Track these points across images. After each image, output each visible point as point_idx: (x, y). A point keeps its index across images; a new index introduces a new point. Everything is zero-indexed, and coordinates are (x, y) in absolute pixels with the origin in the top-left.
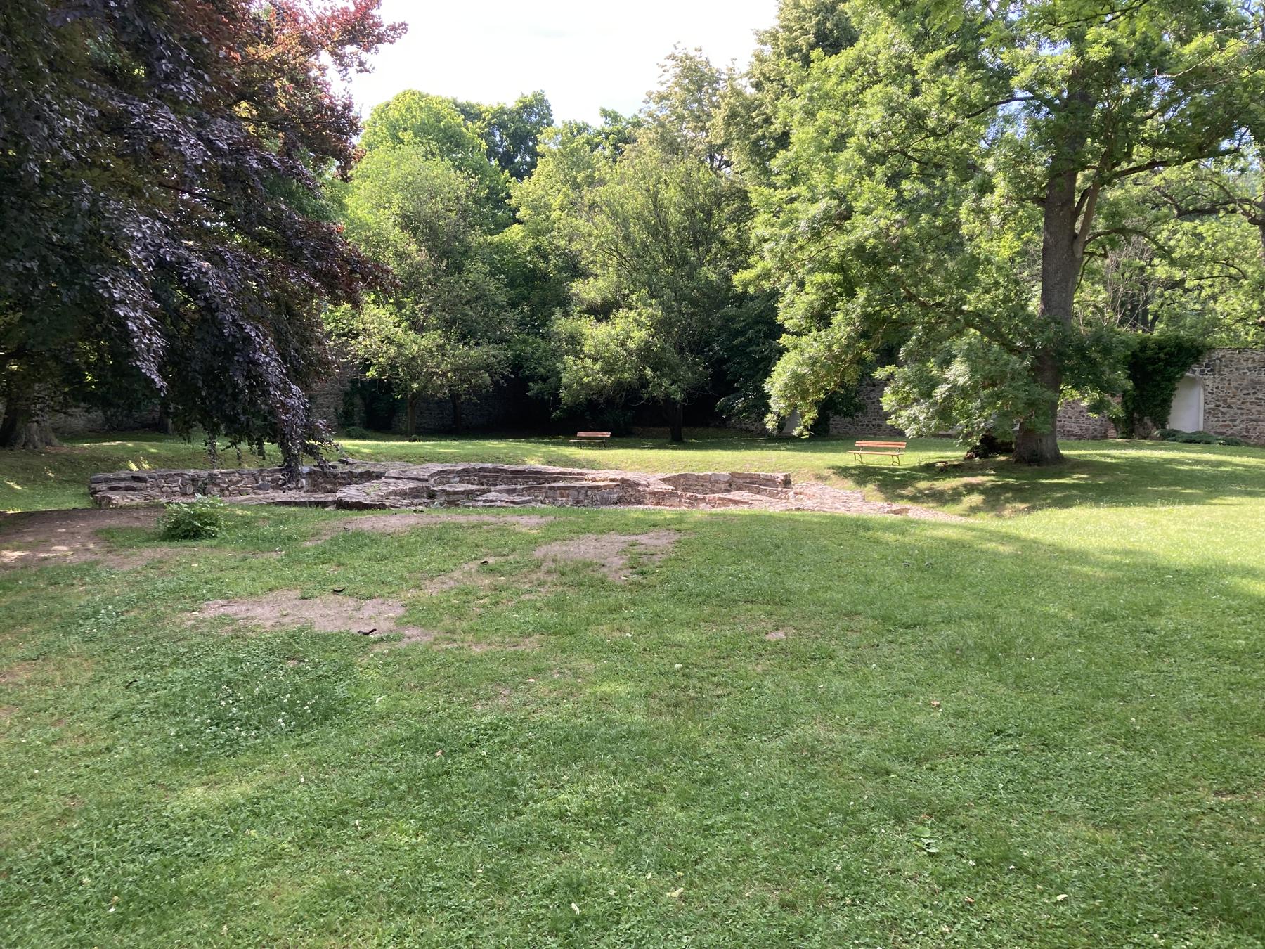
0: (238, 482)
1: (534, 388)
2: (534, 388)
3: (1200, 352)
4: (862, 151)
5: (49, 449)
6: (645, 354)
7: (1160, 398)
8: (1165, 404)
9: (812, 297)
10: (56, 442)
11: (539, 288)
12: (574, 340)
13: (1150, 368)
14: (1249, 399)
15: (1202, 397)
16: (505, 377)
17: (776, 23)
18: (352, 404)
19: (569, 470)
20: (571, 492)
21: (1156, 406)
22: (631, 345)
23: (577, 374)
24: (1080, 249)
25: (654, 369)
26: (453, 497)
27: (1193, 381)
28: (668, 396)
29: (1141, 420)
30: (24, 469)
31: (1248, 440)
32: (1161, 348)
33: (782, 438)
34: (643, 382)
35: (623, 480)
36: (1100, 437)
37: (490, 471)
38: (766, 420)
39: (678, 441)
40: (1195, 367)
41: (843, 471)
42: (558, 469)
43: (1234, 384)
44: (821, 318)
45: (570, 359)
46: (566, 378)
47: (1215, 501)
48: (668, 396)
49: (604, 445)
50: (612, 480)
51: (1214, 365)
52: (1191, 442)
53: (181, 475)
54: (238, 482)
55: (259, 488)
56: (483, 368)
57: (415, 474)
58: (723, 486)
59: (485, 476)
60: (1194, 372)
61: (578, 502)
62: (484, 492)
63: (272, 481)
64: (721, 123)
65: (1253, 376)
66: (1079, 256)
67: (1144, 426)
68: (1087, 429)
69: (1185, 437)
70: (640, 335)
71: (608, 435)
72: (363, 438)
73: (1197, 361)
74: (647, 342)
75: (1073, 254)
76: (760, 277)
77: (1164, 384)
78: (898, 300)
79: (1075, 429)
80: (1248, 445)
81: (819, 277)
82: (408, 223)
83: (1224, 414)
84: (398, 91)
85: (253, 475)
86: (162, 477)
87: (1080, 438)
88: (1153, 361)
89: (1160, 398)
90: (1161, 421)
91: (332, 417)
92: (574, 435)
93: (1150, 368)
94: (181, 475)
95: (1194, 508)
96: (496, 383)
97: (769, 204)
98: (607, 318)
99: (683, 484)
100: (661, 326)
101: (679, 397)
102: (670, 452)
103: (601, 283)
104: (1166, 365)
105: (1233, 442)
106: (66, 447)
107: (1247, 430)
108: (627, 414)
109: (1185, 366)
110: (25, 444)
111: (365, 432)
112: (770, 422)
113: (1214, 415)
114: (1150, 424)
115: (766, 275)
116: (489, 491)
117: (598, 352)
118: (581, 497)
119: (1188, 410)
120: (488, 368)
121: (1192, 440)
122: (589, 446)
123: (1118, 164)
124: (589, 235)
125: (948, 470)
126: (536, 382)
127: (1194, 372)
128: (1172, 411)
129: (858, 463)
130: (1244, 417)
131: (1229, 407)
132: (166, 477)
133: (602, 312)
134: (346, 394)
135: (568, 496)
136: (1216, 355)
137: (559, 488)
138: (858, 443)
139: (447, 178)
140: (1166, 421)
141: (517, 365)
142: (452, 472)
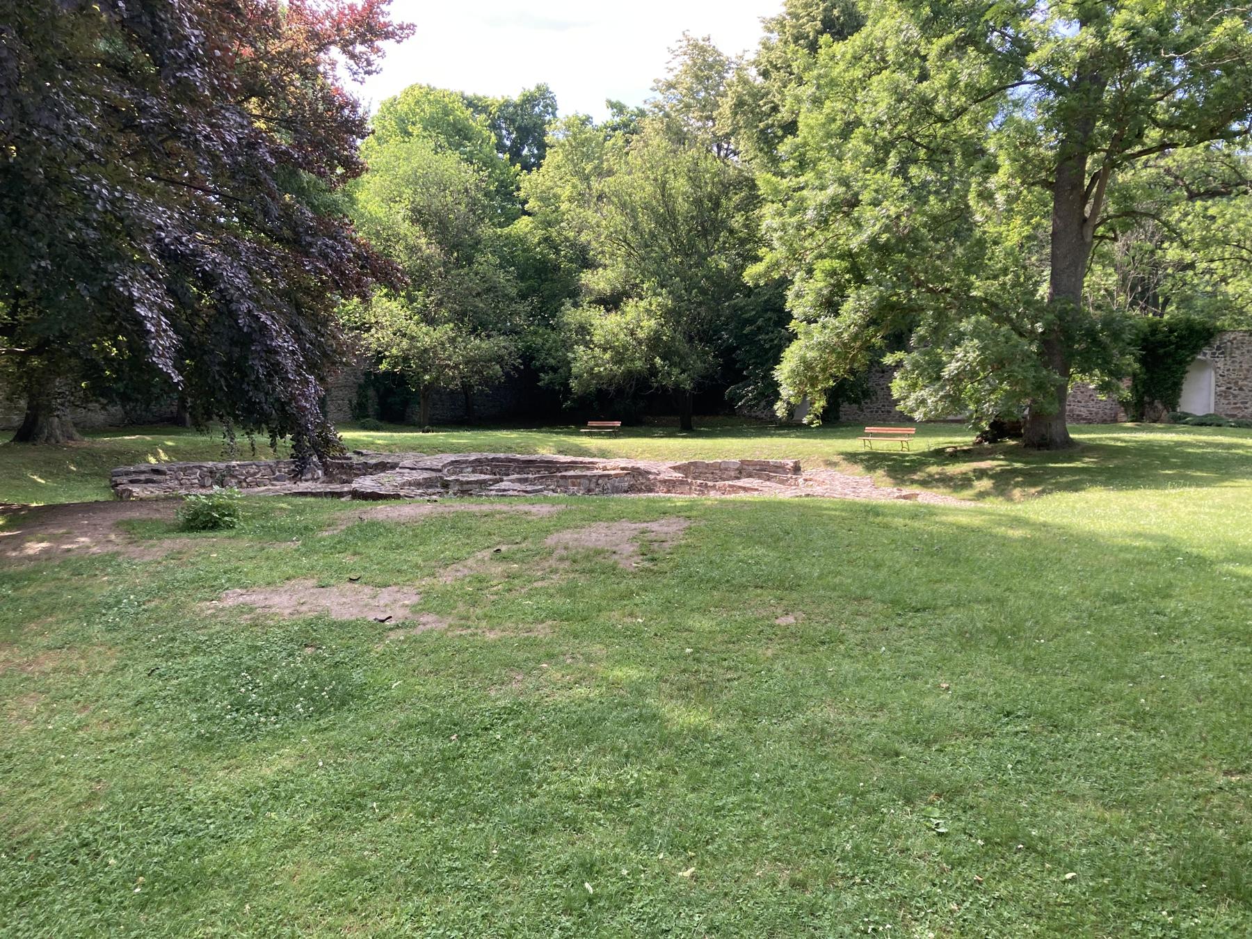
0: (255, 474)
1: (545, 378)
2: (545, 378)
5: (71, 443)
6: (654, 342)
8: (1176, 388)
10: (77, 436)
11: (548, 279)
12: (583, 330)
13: (1161, 351)
15: (1213, 379)
16: (516, 368)
20: (582, 481)
21: (1167, 389)
22: (641, 335)
23: (587, 362)
26: (466, 487)
29: (1151, 403)
30: (47, 463)
35: (633, 469)
36: (1110, 421)
38: (776, 407)
39: (688, 428)
40: (1206, 350)
41: (852, 457)
44: (831, 305)
46: (576, 368)
49: (615, 434)
50: (623, 469)
51: (1225, 348)
52: (1202, 424)
53: (200, 467)
54: (255, 474)
55: (276, 479)
58: (733, 474)
60: (1205, 354)
66: (1088, 240)
67: (1154, 409)
68: (1097, 413)
71: (618, 424)
73: (1208, 343)
75: (1083, 238)
77: (1175, 367)
78: (909, 291)
83: (1235, 396)
85: (270, 467)
87: (1089, 421)
88: (1163, 344)
90: (1172, 403)
91: (346, 409)
93: (1161, 351)
94: (200, 467)
96: (507, 374)
99: (693, 471)
101: (688, 386)
103: (610, 274)
104: (1178, 348)
106: (87, 441)
108: (637, 402)
109: (1196, 349)
112: (780, 409)
113: (1225, 398)
114: (1160, 407)
115: (776, 265)
118: (592, 486)
119: (1199, 393)
120: (500, 360)
121: (1202, 423)
122: (599, 435)
126: (546, 373)
127: (1205, 355)
128: (1183, 393)
129: (867, 449)
131: (1241, 389)
133: (612, 302)
134: (360, 386)
135: (579, 484)
137: (571, 477)
138: (868, 429)
141: (528, 356)
142: (465, 462)
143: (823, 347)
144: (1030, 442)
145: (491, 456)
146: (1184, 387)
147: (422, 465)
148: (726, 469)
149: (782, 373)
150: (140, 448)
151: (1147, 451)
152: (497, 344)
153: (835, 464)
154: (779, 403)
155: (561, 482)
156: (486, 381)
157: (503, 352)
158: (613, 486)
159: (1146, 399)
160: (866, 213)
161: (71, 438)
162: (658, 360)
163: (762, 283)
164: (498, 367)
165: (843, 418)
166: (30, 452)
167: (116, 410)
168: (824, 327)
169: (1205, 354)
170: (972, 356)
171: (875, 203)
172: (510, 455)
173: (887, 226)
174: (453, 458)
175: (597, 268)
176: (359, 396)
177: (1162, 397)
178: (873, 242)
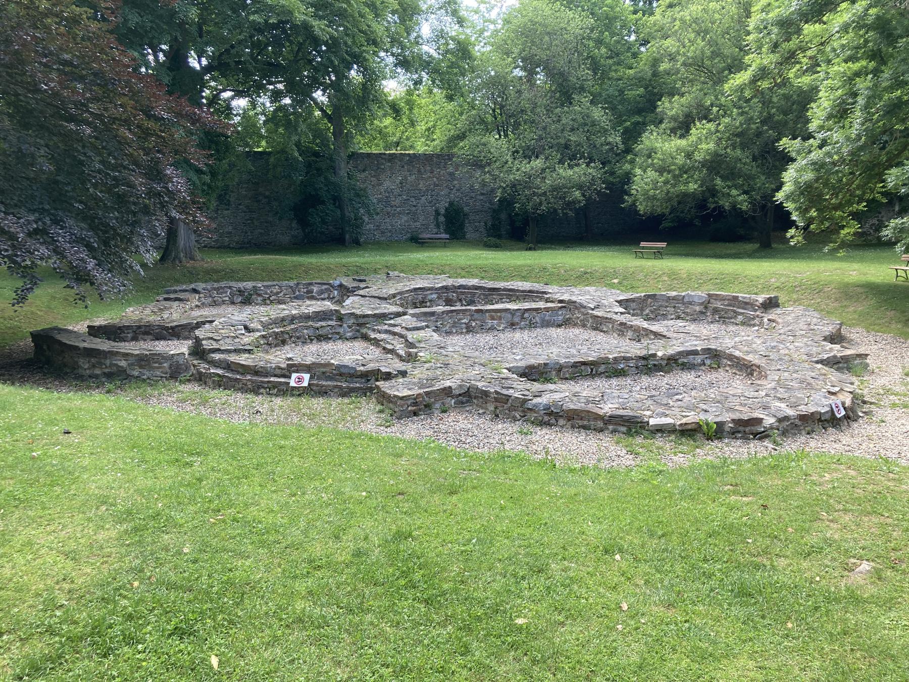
6: (715, 164)
16: (599, 193)
18: (499, 219)
19: (462, 281)
20: (503, 314)
22: (698, 156)
23: (645, 184)
26: (361, 321)
28: (734, 206)
38: (788, 235)
41: (875, 290)
42: (526, 285)
47: (230, 324)
48: (734, 206)
49: (659, 254)
50: (561, 301)
53: (230, 287)
54: (278, 293)
55: (296, 298)
58: (698, 308)
59: (463, 293)
61: (513, 324)
63: (308, 292)
74: (716, 154)
76: (754, 81)
86: (215, 289)
91: (482, 229)
92: (636, 242)
95: (681, 349)
96: (588, 200)
98: (26, 126)
102: (837, 265)
111: (498, 241)
115: (763, 73)
116: (405, 314)
118: (516, 320)
132: (217, 289)
134: (494, 211)
135: (500, 318)
138: (643, 244)
143: (818, 166)
148: (690, 303)
152: (578, 174)
154: (792, 231)
155: (476, 316)
158: (543, 320)
162: (718, 181)
165: (468, 236)
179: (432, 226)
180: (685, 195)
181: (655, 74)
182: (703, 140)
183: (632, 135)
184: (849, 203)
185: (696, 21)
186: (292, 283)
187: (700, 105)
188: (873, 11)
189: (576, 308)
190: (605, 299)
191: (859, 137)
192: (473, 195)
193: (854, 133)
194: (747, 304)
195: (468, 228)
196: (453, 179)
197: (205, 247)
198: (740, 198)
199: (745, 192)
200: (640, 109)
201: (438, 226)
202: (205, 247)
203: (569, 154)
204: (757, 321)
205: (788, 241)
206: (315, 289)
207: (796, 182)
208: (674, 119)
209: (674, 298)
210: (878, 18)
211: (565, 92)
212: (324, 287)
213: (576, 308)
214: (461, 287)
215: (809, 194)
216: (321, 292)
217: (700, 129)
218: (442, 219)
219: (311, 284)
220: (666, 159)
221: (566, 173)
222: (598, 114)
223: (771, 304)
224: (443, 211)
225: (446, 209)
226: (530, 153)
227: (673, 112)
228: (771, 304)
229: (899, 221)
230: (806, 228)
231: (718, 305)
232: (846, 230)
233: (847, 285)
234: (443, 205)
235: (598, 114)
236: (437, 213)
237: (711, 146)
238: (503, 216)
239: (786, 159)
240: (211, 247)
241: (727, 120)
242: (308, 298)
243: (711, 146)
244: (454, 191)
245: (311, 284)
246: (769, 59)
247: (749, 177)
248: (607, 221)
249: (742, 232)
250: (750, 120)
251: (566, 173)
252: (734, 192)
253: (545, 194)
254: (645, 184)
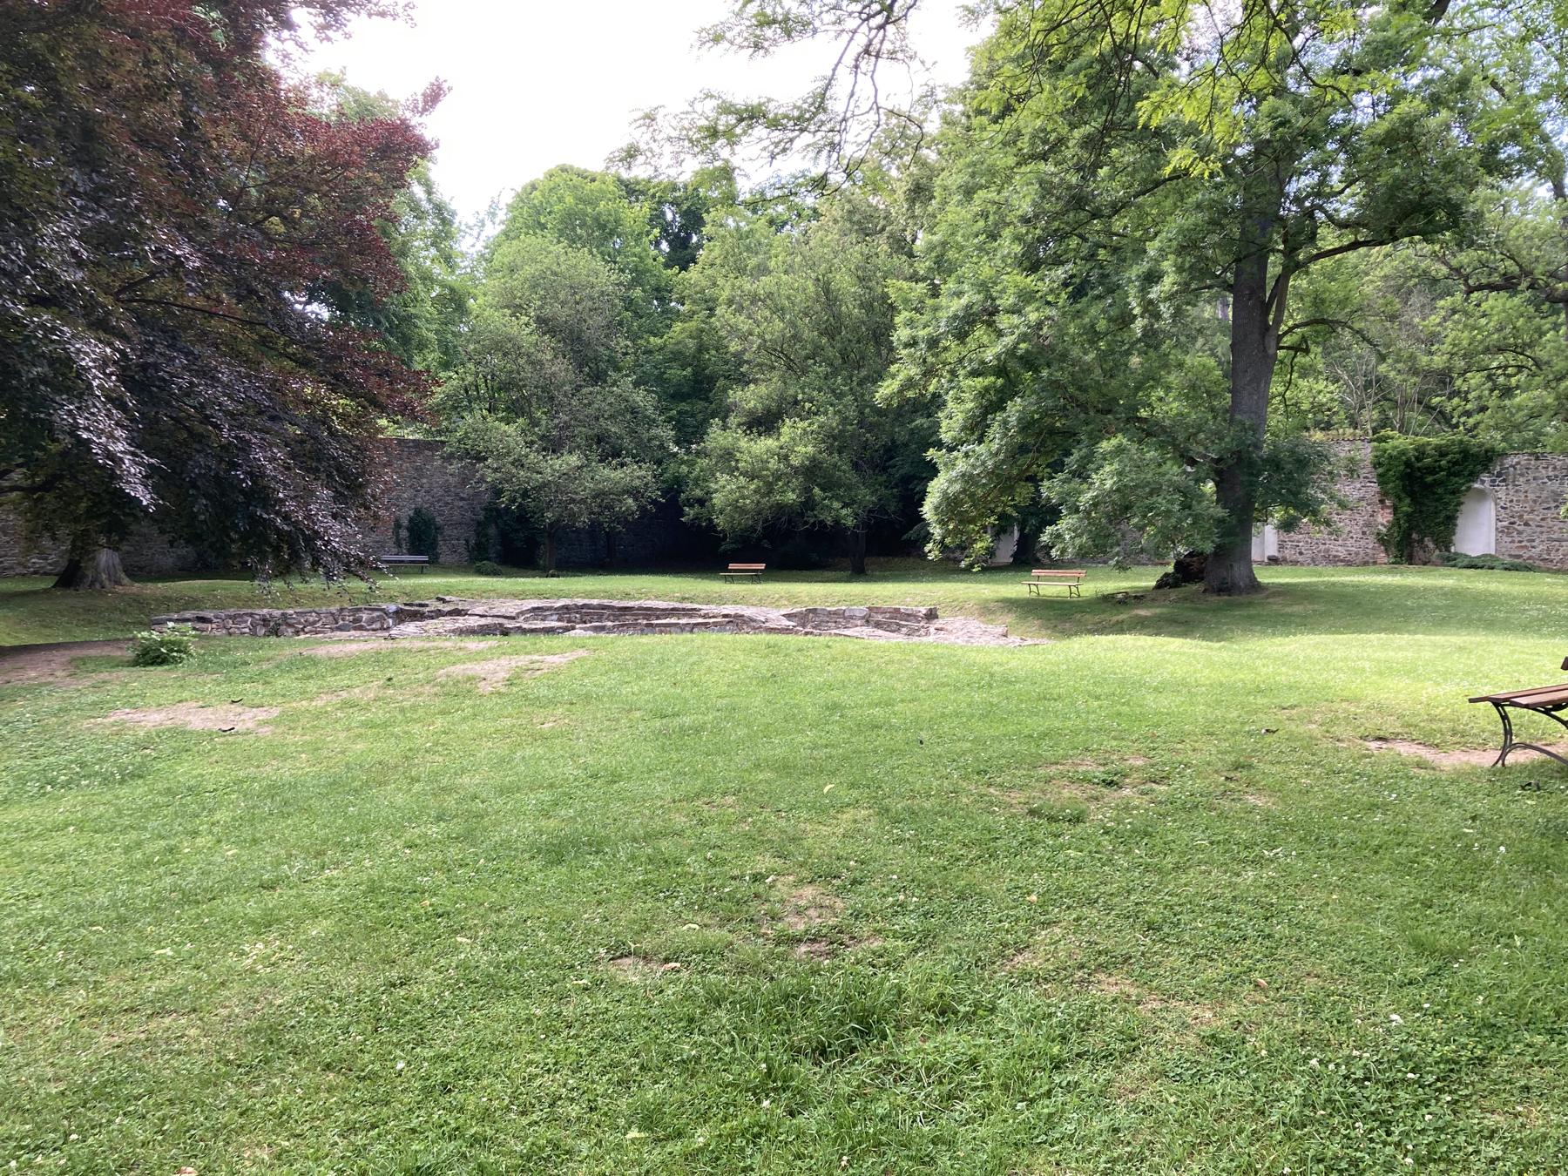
0: (315, 622)
1: (690, 513)
2: (690, 513)
3: (1490, 460)
4: (1018, 238)
5: (119, 589)
6: (812, 471)
7: (1442, 515)
8: (1450, 522)
9: (971, 405)
10: (126, 580)
11: (695, 390)
12: (728, 455)
13: (1430, 479)
14: (1549, 514)
15: (1493, 513)
16: (654, 502)
17: (967, 77)
18: (486, 535)
21: (1438, 524)
22: (795, 461)
23: (727, 494)
24: (1273, 344)
25: (823, 490)
27: (1482, 494)
28: (837, 522)
29: (1421, 541)
30: (87, 610)
31: (1550, 565)
32: (1443, 455)
33: (950, 566)
34: (809, 504)
35: (737, 616)
36: (1366, 563)
37: (594, 607)
38: (926, 549)
39: (859, 572)
40: (1485, 477)
41: (1011, 605)
43: (1531, 496)
44: (977, 428)
45: (723, 478)
46: (718, 500)
48: (837, 522)
49: (757, 578)
50: (725, 616)
51: (1507, 474)
52: (1475, 567)
53: (251, 615)
54: (315, 622)
55: (340, 629)
56: (627, 492)
57: (503, 611)
59: (587, 614)
60: (1483, 482)
62: (567, 629)
64: (902, 197)
65: (1554, 486)
66: (1271, 352)
67: (1424, 548)
68: (1357, 554)
69: (1466, 562)
70: (805, 450)
71: (762, 566)
72: (495, 573)
73: (1486, 469)
74: (813, 459)
75: (1265, 350)
77: (1448, 497)
78: (1061, 408)
79: (1342, 553)
80: (1548, 570)
81: (980, 382)
82: (545, 324)
83: (1520, 533)
84: (552, 164)
86: (230, 617)
87: (1348, 563)
88: (1432, 470)
89: (1442, 515)
90: (1444, 541)
93: (1430, 479)
94: (251, 615)
96: (642, 509)
97: (906, 301)
99: (809, 619)
100: (834, 440)
101: (850, 522)
103: (763, 389)
104: (1449, 475)
105: (1517, 566)
106: (136, 587)
107: (1549, 551)
108: (790, 543)
109: (1473, 476)
110: (92, 584)
112: (932, 551)
113: (1508, 534)
114: (1431, 546)
115: (910, 383)
117: (753, 469)
119: (1478, 531)
120: (634, 493)
121: (1473, 565)
122: (741, 580)
123: (103, 467)
124: (742, 330)
125: (1137, 598)
126: (691, 506)
127: (1483, 483)
128: (1458, 530)
129: (1033, 595)
130: (1544, 536)
131: (1526, 524)
133: (764, 423)
134: (479, 523)
136: (1509, 461)
138: (732, 566)
139: (593, 270)
140: (1451, 542)
141: (674, 488)
142: (550, 609)
143: (967, 478)
144: (1209, 585)
145: (580, 602)
146: (1459, 522)
147: (494, 612)
148: (851, 617)
149: (928, 510)
150: (194, 594)
151: (1454, 595)
152: (632, 474)
153: (992, 612)
154: (930, 546)
156: (622, 519)
157: (637, 483)
159: (1414, 536)
160: (1004, 321)
161: (118, 582)
162: (816, 490)
163: (895, 403)
164: (630, 501)
165: (442, 559)
166: (72, 599)
167: (186, 551)
168: (967, 455)
169: (1483, 482)
170: (1109, 484)
171: (1015, 310)
172: (606, 602)
173: (1025, 334)
174: (536, 603)
175: (748, 383)
176: (478, 534)
177: (1432, 535)
178: (1011, 352)
179: (391, 544)
180: (780, 507)
181: (701, 348)
182: (796, 440)
183: (690, 433)
184: (982, 515)
185: (770, 295)
186: (333, 609)
187: (782, 398)
188: (1022, 346)
189: (745, 622)
190: (776, 616)
191: (999, 450)
192: (449, 499)
193: (994, 447)
194: (909, 616)
195: (443, 548)
196: (422, 476)
197: (35, 572)
198: (844, 512)
199: (845, 506)
200: (695, 390)
201: (398, 544)
202: (35, 572)
203: (611, 452)
204: (922, 632)
205: (926, 555)
206: (365, 617)
207: (945, 493)
208: (751, 413)
209: (835, 613)
210: (1027, 351)
211: (594, 369)
212: (376, 614)
213: (745, 622)
214: (584, 606)
215: (950, 506)
216: (372, 621)
217: (789, 429)
218: (404, 533)
219: (360, 610)
220: (748, 460)
221: (612, 475)
222: (643, 399)
223: (931, 615)
224: (405, 522)
225: (411, 520)
226: (553, 446)
227: (752, 404)
228: (931, 615)
229: (1054, 528)
230: (942, 542)
231: (880, 618)
232: (979, 545)
233: (986, 601)
234: (405, 514)
235: (643, 399)
236: (398, 525)
237: (810, 449)
238: (492, 531)
239: (932, 470)
240: (46, 574)
241: (822, 419)
242: (355, 629)
243: (810, 449)
244: (422, 493)
245: (360, 610)
246: (914, 371)
247: (849, 488)
248: (673, 538)
249: (815, 557)
250: (845, 420)
251: (612, 475)
252: (836, 505)
253: (583, 501)
254: (727, 494)
